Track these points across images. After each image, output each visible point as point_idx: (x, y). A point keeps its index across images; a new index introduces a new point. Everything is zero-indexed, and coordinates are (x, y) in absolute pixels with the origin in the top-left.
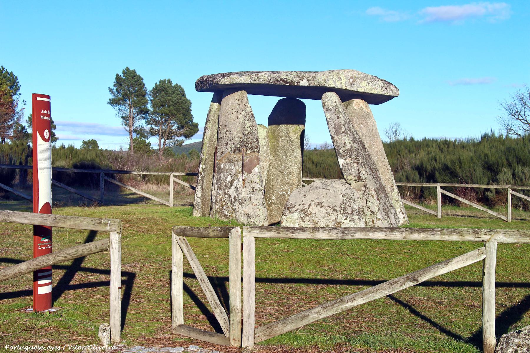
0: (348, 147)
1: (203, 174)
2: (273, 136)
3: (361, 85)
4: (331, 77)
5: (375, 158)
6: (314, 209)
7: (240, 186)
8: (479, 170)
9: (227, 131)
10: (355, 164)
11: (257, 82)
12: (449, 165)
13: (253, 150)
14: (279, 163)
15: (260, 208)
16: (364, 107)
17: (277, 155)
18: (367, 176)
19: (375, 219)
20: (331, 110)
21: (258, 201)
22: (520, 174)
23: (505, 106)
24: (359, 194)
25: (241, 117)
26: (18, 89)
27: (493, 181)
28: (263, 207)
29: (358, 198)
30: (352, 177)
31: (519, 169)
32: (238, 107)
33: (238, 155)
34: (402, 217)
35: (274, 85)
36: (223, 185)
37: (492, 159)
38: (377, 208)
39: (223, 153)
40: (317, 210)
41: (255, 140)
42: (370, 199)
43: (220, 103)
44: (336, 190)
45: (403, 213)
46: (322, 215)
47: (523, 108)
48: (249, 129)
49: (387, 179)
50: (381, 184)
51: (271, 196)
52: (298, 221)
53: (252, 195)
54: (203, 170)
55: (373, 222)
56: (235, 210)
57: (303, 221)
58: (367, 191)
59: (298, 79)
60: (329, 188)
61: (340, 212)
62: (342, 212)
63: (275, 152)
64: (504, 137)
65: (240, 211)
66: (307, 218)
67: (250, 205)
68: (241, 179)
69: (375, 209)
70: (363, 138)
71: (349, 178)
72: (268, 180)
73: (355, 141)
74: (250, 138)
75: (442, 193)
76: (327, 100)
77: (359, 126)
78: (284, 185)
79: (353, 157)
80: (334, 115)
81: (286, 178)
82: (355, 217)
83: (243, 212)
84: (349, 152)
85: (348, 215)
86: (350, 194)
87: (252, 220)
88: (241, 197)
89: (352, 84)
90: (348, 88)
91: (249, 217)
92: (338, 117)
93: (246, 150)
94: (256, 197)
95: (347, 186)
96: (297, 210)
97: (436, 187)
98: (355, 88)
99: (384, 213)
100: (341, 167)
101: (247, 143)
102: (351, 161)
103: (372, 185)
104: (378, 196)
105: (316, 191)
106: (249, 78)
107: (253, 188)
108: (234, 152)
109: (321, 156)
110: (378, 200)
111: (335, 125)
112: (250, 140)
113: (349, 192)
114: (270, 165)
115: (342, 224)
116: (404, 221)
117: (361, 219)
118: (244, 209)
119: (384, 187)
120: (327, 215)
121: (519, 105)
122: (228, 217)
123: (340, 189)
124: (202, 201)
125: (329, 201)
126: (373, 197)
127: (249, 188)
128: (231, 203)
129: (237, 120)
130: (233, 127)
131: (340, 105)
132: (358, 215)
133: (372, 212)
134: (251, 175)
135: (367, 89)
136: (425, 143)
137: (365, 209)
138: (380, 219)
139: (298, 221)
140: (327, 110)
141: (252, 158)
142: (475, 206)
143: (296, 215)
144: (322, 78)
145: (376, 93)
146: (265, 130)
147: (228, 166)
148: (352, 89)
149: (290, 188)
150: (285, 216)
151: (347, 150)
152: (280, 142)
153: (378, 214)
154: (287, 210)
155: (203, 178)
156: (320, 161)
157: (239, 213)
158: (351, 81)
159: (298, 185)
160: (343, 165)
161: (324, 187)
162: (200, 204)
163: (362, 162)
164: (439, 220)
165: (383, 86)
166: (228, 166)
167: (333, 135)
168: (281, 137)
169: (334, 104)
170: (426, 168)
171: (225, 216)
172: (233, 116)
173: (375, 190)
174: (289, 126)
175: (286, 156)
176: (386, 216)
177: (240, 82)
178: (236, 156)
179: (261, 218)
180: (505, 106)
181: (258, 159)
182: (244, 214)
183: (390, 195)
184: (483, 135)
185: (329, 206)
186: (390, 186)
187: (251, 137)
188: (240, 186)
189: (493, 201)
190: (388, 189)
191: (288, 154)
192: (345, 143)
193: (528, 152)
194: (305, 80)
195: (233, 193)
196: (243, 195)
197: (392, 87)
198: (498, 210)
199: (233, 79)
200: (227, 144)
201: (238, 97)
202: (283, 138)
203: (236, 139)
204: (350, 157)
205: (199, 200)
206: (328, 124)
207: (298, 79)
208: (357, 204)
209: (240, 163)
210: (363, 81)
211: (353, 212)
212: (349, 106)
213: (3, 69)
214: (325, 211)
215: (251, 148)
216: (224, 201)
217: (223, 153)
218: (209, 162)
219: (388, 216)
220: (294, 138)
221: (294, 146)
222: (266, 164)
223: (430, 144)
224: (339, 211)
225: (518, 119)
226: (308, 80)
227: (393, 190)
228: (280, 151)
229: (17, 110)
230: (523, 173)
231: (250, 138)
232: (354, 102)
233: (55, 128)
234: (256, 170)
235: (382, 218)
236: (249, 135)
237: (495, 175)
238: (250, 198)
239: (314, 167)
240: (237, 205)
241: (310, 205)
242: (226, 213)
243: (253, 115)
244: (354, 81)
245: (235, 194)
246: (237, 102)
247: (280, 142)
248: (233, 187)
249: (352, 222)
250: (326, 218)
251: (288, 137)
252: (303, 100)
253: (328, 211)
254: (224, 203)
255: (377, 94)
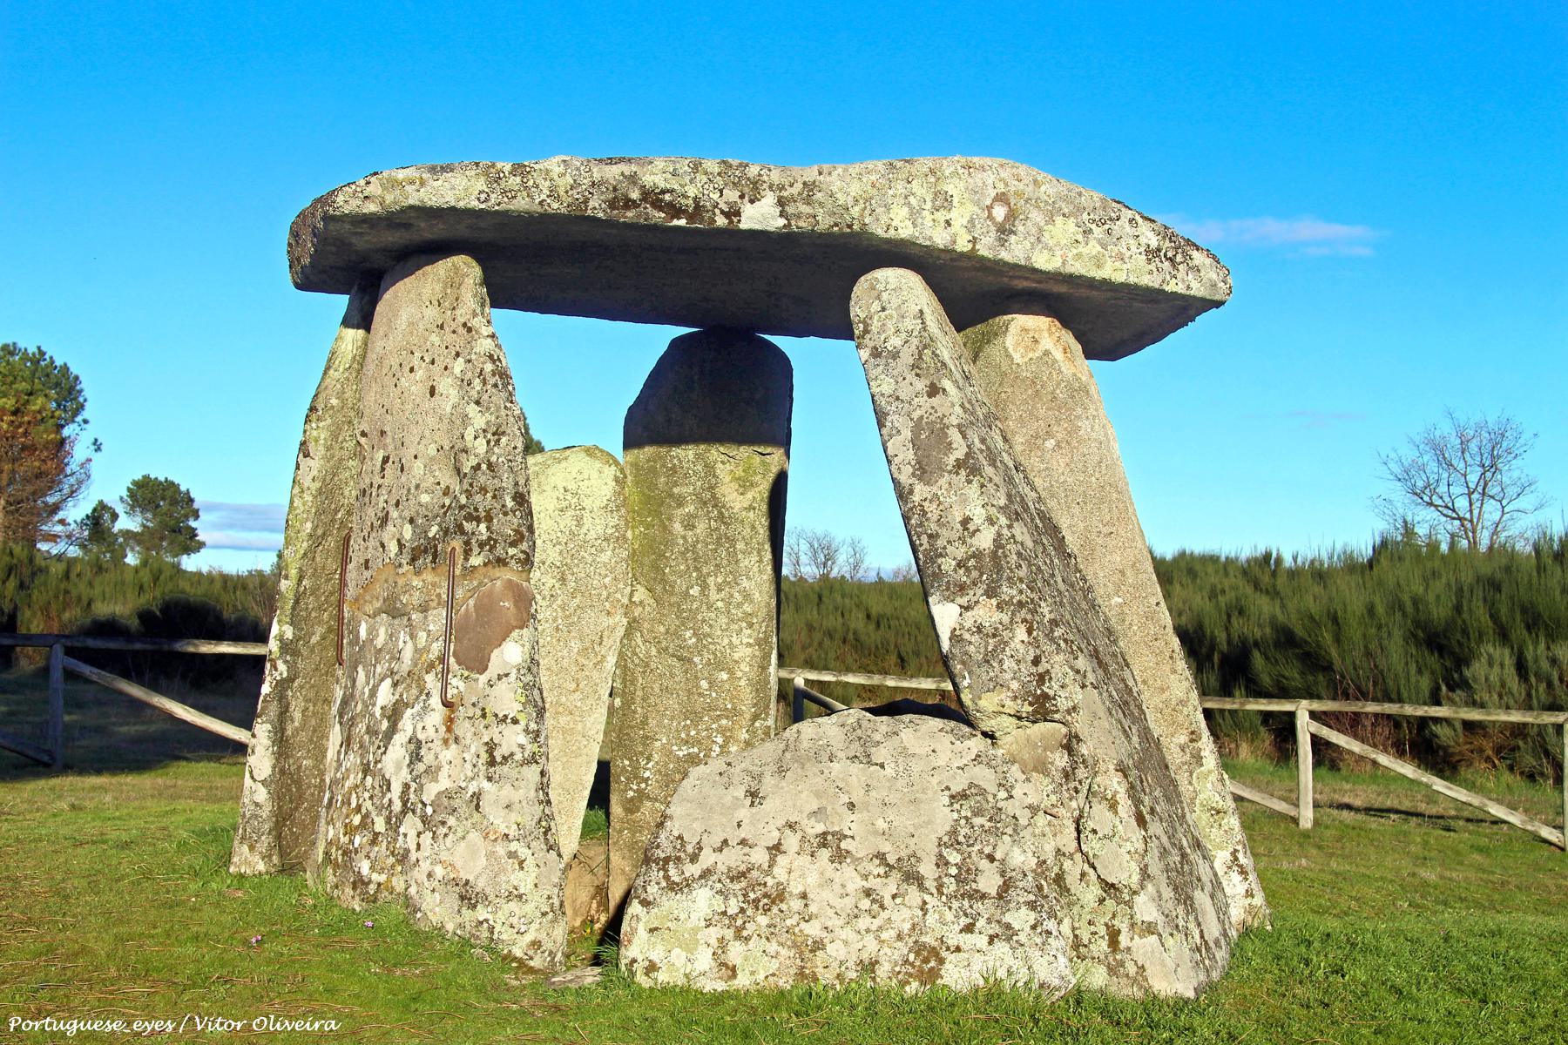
0: (985, 540)
1: (282, 667)
2: (647, 500)
3: (1046, 238)
4: (900, 188)
5: (1111, 603)
6: (801, 872)
7: (431, 732)
8: (1397, 655)
9: (386, 460)
10: (1021, 633)
11: (521, 204)
12: (1299, 631)
13: (499, 551)
14: (672, 620)
15: (523, 852)
16: (1058, 355)
17: (664, 581)
18: (1079, 695)
19: (1124, 927)
20: (895, 355)
21: (514, 817)
22: (1545, 665)
23: (1397, 470)
24: (1032, 791)
25: (447, 386)
26: (82, 407)
27: (1451, 688)
28: (539, 845)
29: (1034, 809)
30: (1005, 696)
31: (1537, 651)
32: (435, 338)
33: (429, 576)
34: (1241, 888)
35: (609, 223)
36: (361, 727)
37: (1440, 612)
38: (1134, 868)
39: (366, 565)
40: (812, 879)
41: (510, 504)
42: (1099, 817)
43: (368, 330)
44: (916, 767)
45: (1243, 872)
46: (839, 903)
47: (1445, 475)
48: (481, 446)
49: (1166, 702)
50: (1146, 734)
51: (636, 767)
52: (713, 934)
53: (486, 785)
54: (285, 647)
55: (1114, 942)
56: (403, 858)
57: (738, 935)
58: (1081, 773)
59: (732, 195)
60: (879, 754)
61: (940, 888)
62: (951, 886)
63: (656, 568)
64: (1444, 547)
65: (425, 866)
66: (763, 920)
67: (474, 836)
68: (435, 701)
69: (1125, 872)
70: (1051, 503)
71: (988, 702)
72: (623, 695)
73: (1016, 510)
74: (483, 490)
75: (1313, 736)
76: (876, 306)
77: (1034, 443)
78: (693, 716)
79: (1007, 591)
80: (910, 377)
81: (704, 684)
82: (1021, 918)
83: (439, 871)
84: (990, 569)
85: (978, 906)
86: (992, 788)
87: (482, 913)
88: (431, 791)
89: (1005, 231)
90: (983, 251)
91: (468, 897)
92: (933, 391)
93: (467, 553)
94: (507, 792)
95: (977, 744)
96: (706, 874)
97: (1292, 715)
98: (1016, 252)
99: (1168, 893)
100: (946, 645)
101: (469, 518)
102: (997, 616)
103: (1103, 742)
104: (1137, 803)
105: (812, 769)
106: (481, 184)
107: (491, 747)
108: (413, 560)
109: (891, 598)
110: (1141, 821)
111: (918, 427)
112: (483, 502)
113: (985, 777)
114: (633, 626)
115: (950, 957)
116: (1250, 910)
117: (1050, 925)
118: (444, 856)
119: (1158, 743)
120: (865, 904)
121: (1433, 466)
122: (372, 888)
123: (941, 761)
124: (277, 797)
125: (881, 824)
126: (1113, 806)
127: (476, 747)
128: (388, 820)
129: (427, 404)
130: (412, 439)
131: (948, 343)
132: (1032, 906)
133: (1109, 887)
134: (483, 678)
135: (1079, 256)
136: (1183, 565)
137: (1073, 869)
138: (1150, 929)
139: (713, 934)
140: (876, 353)
141: (490, 594)
142: (1384, 759)
143: (703, 900)
144: (855, 189)
145: (1120, 277)
146: (611, 471)
147: (382, 631)
148: (1004, 255)
149: (722, 731)
150: (645, 903)
151: (977, 555)
152: (677, 527)
153: (1140, 900)
154: (656, 874)
155: (282, 686)
156: (889, 611)
157: (419, 874)
158: (1000, 212)
159: (755, 717)
160: (955, 638)
161: (856, 748)
162: (265, 812)
163: (1054, 623)
164: (1306, 835)
165: (1154, 244)
166: (382, 631)
167: (904, 479)
168: (681, 503)
169: (911, 324)
170: (1213, 638)
171: (360, 883)
172: (414, 386)
173: (1122, 770)
174: (715, 453)
175: (704, 587)
176: (1181, 910)
177: (433, 201)
178: (422, 583)
179: (529, 908)
180: (1397, 470)
181: (524, 600)
182: (445, 882)
183: (1182, 779)
184: (1378, 542)
185: (881, 857)
186: (1183, 739)
187: (492, 484)
188: (431, 732)
189: (1453, 754)
190: (1174, 756)
191: (711, 581)
192: (966, 521)
193: (1563, 591)
194: (768, 201)
195: (398, 768)
196: (444, 783)
197: (1195, 254)
198: (1471, 786)
199: (394, 184)
200: (385, 520)
201: (438, 287)
202: (690, 509)
203: (425, 498)
204: (991, 593)
205: (262, 795)
206: (881, 425)
207: (732, 195)
208: (1029, 847)
209: (437, 620)
210: (1059, 220)
211: (1006, 886)
212: (988, 349)
213: (43, 354)
214: (855, 884)
215: (489, 544)
216: (358, 809)
217: (366, 565)
218: (320, 609)
219: (1187, 901)
220: (737, 506)
221: (740, 546)
222: (608, 621)
223: (1198, 567)
224: (930, 884)
225: (1431, 504)
226: (781, 202)
227: (1198, 758)
228: (676, 565)
229: (73, 465)
230: (1554, 661)
231: (483, 490)
232: (1013, 329)
233: (197, 517)
234: (511, 653)
235: (1161, 920)
236: (483, 478)
237: (1459, 669)
238: (477, 796)
239: (872, 627)
240: (412, 834)
241: (776, 849)
242: (365, 867)
243: (504, 375)
244: (1012, 215)
245: (405, 775)
246: (432, 313)
247: (677, 527)
248: (400, 739)
249: (1001, 948)
250: (864, 922)
251: (711, 500)
252: (781, 342)
253: (872, 883)
254: (357, 820)
255: (1125, 286)
